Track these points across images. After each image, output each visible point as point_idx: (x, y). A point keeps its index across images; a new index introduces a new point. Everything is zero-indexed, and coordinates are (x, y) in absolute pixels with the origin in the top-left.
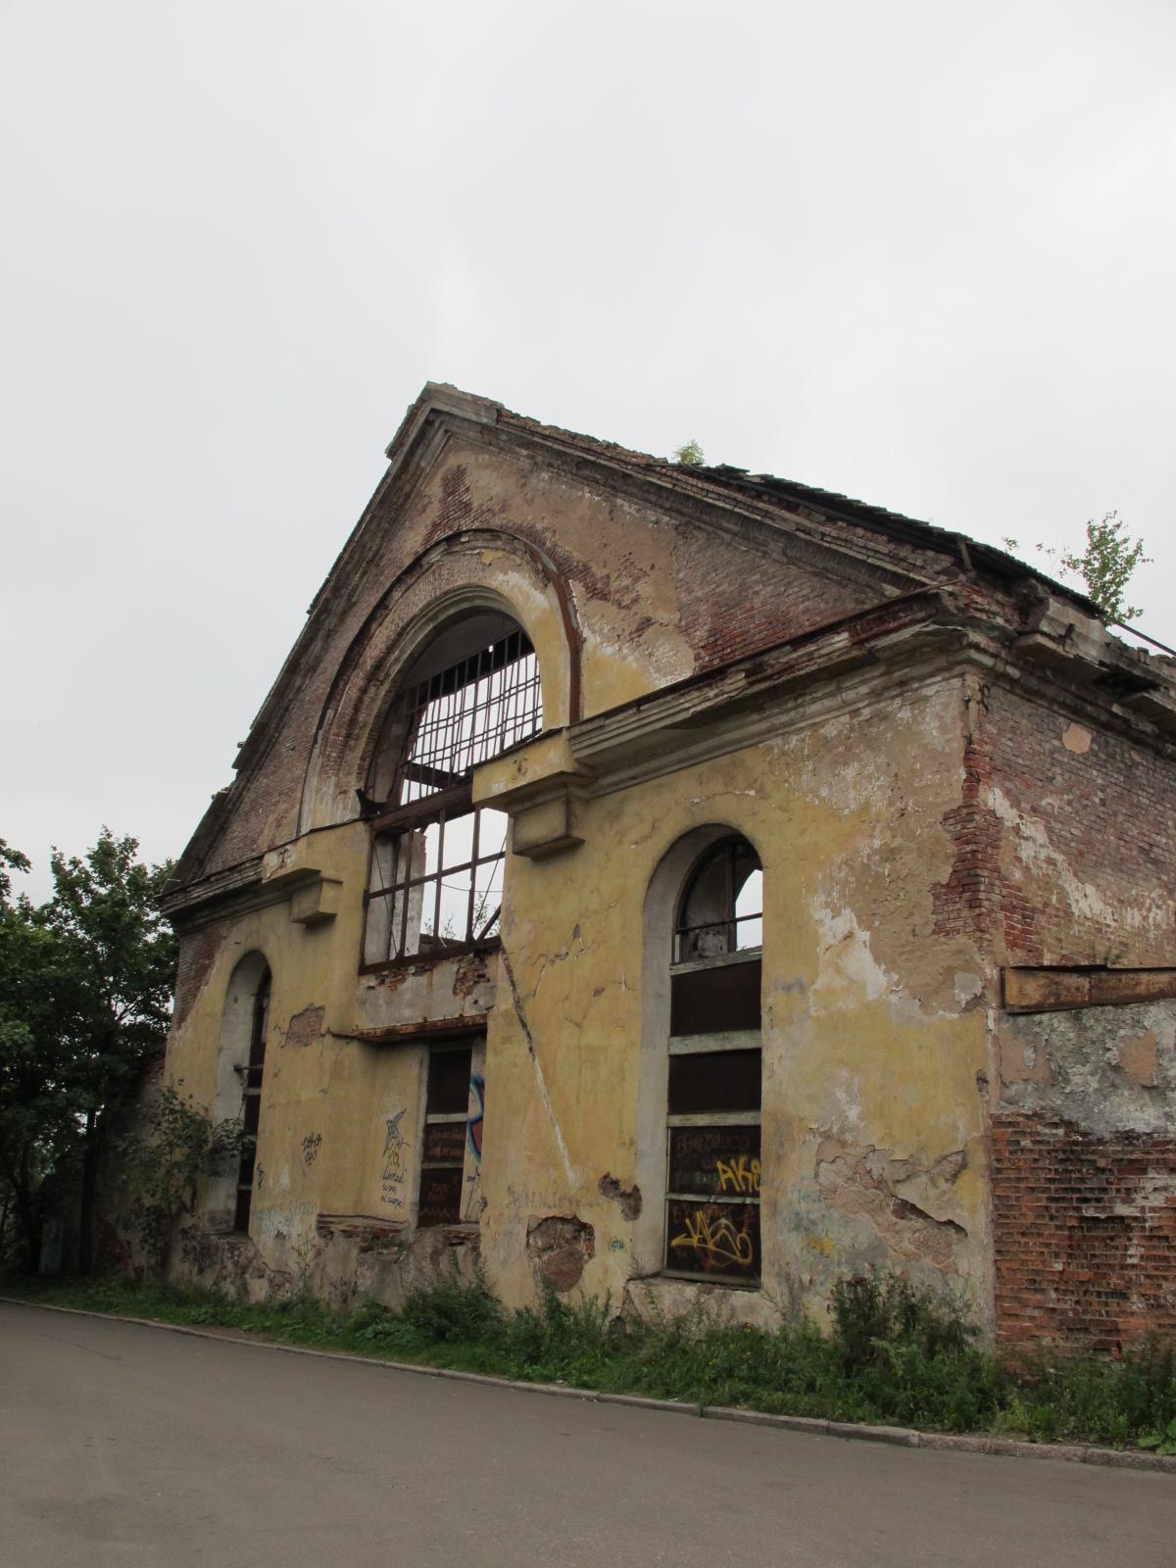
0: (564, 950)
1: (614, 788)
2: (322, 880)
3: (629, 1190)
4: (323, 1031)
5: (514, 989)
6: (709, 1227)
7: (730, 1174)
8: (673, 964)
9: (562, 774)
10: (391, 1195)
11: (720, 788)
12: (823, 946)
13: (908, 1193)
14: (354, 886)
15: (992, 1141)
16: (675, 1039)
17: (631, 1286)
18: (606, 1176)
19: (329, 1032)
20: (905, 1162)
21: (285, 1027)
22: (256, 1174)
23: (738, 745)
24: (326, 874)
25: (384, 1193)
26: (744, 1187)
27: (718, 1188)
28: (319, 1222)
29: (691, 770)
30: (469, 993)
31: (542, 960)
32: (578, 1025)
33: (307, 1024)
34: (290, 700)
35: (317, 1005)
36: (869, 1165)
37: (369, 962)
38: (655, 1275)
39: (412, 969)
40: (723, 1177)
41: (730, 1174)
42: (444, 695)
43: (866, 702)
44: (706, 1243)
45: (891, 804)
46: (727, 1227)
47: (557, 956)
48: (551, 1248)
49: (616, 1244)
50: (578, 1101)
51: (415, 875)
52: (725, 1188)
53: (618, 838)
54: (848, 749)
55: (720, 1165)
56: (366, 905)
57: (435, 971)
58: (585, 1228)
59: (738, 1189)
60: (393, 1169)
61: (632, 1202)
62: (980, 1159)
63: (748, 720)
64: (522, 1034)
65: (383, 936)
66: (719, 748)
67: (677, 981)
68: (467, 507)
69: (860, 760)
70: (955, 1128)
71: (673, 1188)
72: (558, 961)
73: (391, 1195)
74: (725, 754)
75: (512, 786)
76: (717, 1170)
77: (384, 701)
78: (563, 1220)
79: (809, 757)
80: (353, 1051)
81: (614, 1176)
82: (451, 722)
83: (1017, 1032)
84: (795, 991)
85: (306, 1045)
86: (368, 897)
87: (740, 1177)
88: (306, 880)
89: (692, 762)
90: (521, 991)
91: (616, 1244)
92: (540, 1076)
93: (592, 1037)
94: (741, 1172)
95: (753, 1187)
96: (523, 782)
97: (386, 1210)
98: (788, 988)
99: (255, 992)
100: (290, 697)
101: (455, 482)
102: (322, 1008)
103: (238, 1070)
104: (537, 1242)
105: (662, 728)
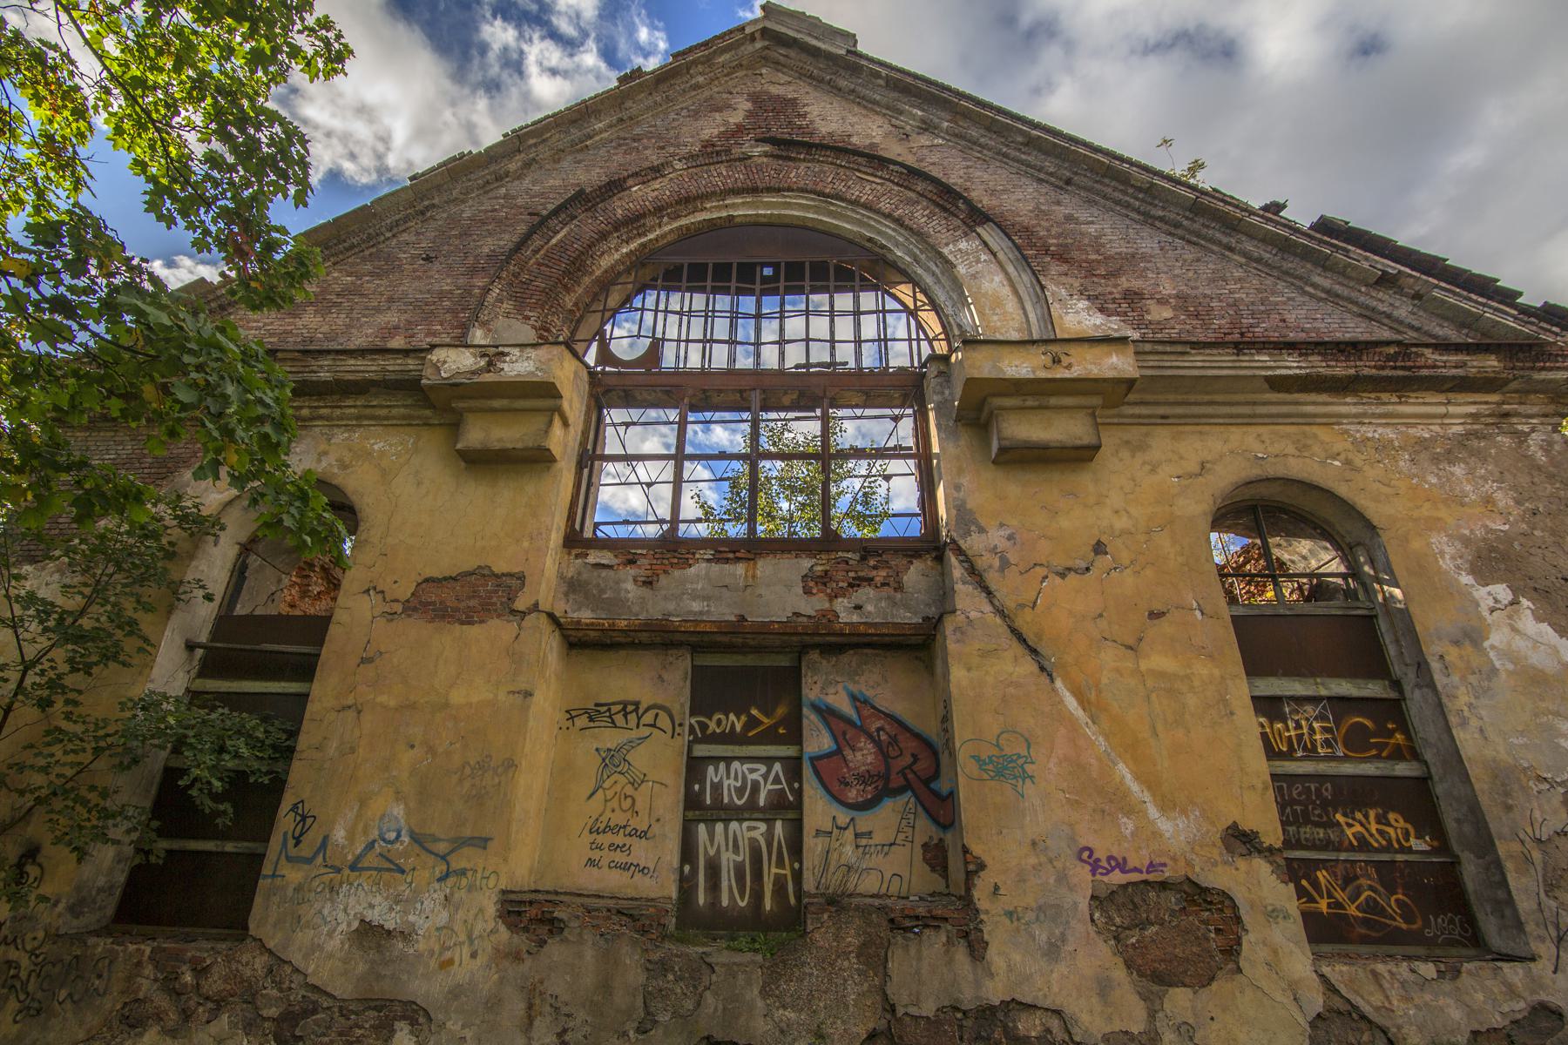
1: (1136, 421)
6: (1343, 890)
7: (1358, 828)
10: (620, 857)
18: (1235, 825)
19: (535, 608)
21: (405, 590)
23: (1310, 420)
25: (596, 855)
26: (1384, 843)
27: (1347, 843)
28: (503, 902)
31: (1041, 571)
34: (433, 206)
35: (500, 567)
40: (1349, 832)
41: (1358, 828)
43: (1462, 421)
44: (1343, 907)
46: (1371, 888)
47: (1069, 569)
48: (1143, 925)
52: (1355, 843)
53: (1148, 467)
55: (1339, 817)
57: (760, 563)
59: (1376, 845)
60: (619, 819)
63: (1348, 400)
64: (1018, 648)
72: (1072, 576)
73: (620, 857)
74: (1293, 424)
75: (1043, 374)
76: (1338, 824)
78: (1163, 885)
81: (1246, 826)
85: (462, 623)
87: (1374, 832)
92: (1071, 702)
93: (1158, 661)
94: (1373, 827)
95: (1398, 841)
96: (1060, 373)
98: (1456, 643)
99: (243, 539)
100: (436, 201)
102: (521, 577)
103: (190, 647)
104: (1110, 918)
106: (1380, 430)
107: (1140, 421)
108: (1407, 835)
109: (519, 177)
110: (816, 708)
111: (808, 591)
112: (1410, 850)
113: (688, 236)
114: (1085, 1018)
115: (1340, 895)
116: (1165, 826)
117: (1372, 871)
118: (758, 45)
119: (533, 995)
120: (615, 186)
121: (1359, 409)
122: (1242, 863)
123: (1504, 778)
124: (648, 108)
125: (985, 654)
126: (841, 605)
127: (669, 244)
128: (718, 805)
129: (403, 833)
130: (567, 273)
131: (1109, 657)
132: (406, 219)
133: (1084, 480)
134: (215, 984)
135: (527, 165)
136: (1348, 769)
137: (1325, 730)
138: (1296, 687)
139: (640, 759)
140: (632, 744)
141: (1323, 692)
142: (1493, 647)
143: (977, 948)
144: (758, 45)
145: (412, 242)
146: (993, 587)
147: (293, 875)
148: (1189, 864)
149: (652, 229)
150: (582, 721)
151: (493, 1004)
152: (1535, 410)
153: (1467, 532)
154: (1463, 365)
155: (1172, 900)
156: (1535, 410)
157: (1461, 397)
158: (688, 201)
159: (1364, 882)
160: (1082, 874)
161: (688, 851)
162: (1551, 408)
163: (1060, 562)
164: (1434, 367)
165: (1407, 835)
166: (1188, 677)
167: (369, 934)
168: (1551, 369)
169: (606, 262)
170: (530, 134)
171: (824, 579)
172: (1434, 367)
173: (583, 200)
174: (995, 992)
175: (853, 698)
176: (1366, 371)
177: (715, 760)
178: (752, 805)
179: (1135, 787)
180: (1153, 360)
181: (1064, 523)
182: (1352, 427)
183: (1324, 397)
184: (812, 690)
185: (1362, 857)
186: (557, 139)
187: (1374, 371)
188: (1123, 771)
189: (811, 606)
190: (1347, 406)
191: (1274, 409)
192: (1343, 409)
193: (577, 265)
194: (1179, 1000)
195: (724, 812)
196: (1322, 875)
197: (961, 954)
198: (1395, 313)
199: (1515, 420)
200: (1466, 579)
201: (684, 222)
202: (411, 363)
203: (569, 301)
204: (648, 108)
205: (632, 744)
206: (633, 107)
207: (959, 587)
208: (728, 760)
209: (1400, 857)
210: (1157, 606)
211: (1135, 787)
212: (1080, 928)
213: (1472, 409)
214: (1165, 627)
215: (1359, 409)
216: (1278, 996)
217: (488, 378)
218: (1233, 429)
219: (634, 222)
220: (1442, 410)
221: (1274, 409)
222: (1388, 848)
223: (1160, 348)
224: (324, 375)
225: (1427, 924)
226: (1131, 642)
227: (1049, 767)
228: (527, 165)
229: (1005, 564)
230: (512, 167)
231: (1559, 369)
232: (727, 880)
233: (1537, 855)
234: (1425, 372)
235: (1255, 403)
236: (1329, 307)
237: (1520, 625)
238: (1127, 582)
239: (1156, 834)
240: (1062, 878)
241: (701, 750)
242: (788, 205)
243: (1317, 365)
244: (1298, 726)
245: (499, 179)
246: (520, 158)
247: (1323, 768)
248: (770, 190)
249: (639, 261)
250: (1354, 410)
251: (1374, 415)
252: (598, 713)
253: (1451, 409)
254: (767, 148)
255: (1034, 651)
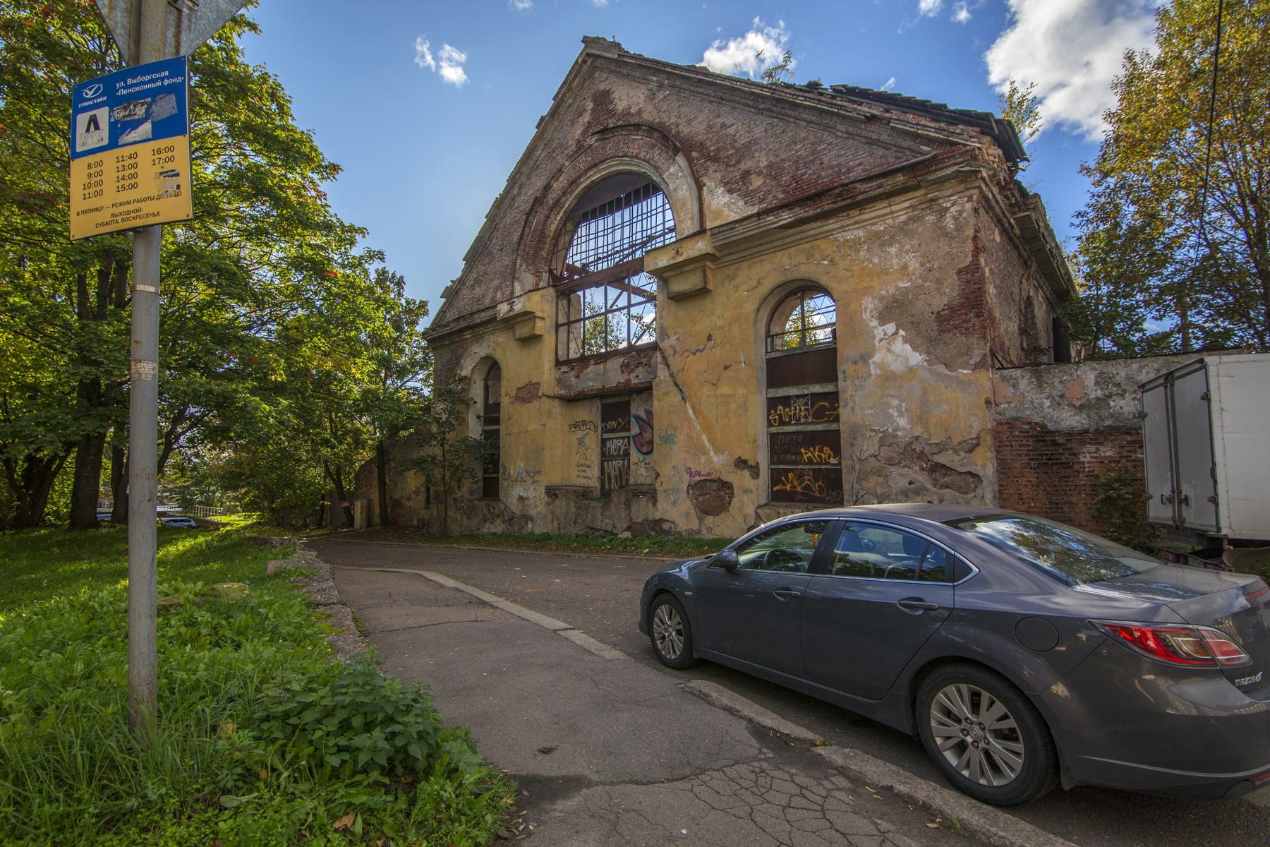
0: (702, 347)
2: (535, 317)
3: (754, 464)
4: (540, 394)
5: (548, 397)
7: (810, 454)
8: (767, 352)
9: (708, 254)
11: (804, 260)
12: (878, 339)
13: (940, 459)
14: (550, 322)
15: (996, 434)
16: (771, 390)
17: (759, 511)
19: (544, 395)
20: (937, 444)
21: (514, 394)
22: (501, 469)
23: (815, 238)
24: (538, 314)
29: (783, 252)
30: (632, 371)
31: (687, 353)
32: (714, 385)
33: (529, 393)
36: (913, 447)
37: (561, 359)
38: (767, 504)
39: (592, 362)
41: (810, 454)
42: (644, 199)
45: (922, 264)
48: (704, 495)
49: (746, 491)
50: (717, 422)
51: (572, 319)
54: (892, 237)
55: (803, 450)
56: (557, 331)
58: (726, 486)
60: (583, 462)
61: (755, 471)
62: (988, 440)
63: (831, 222)
64: (675, 390)
65: (565, 346)
66: (803, 239)
67: (769, 361)
68: (612, 113)
69: (900, 242)
70: (971, 426)
71: (772, 462)
72: (698, 353)
73: (584, 474)
75: (672, 262)
77: (559, 224)
78: (712, 481)
79: (864, 242)
80: (557, 403)
82: (654, 212)
83: (1003, 378)
84: (860, 364)
86: (558, 326)
88: (528, 316)
89: (785, 247)
90: (674, 369)
91: (746, 491)
92: (690, 411)
93: (725, 389)
96: (680, 259)
97: (582, 482)
98: (855, 363)
101: (603, 99)
102: (539, 383)
103: (479, 417)
105: (775, 228)
106: (855, 232)
107: (734, 262)
108: (830, 456)
109: (520, 194)
110: (634, 416)
111: (622, 372)
112: (829, 463)
113: (582, 198)
114: (681, 524)
115: (796, 483)
116: (715, 459)
117: (811, 473)
118: (589, 63)
119: (553, 513)
120: (547, 187)
121: (839, 224)
122: (739, 472)
123: (855, 431)
124: (554, 131)
125: (665, 394)
126: (633, 375)
127: (576, 204)
128: (610, 456)
129: (896, 414)
130: (539, 242)
131: (706, 390)
132: (492, 233)
133: (708, 303)
134: (497, 512)
135: (520, 188)
136: (810, 428)
137: (807, 410)
138: (794, 391)
139: (587, 440)
140: (585, 436)
141: (806, 392)
142: (874, 362)
143: (655, 504)
144: (589, 63)
145: (496, 242)
146: (670, 363)
147: (505, 483)
148: (721, 473)
149: (565, 203)
150: (573, 429)
151: (545, 517)
152: (950, 192)
153: (884, 292)
154: (880, 186)
155: (715, 486)
156: (950, 192)
157: (897, 199)
158: (573, 183)
159: (807, 477)
160: (687, 477)
161: (602, 471)
162: (961, 187)
163: (694, 348)
164: (865, 192)
165: (830, 456)
166: (734, 395)
167: (521, 498)
168: (942, 169)
169: (553, 228)
170: (515, 175)
171: (627, 365)
172: (865, 192)
173: (538, 201)
174: (658, 516)
175: (646, 411)
176: (826, 208)
177: (609, 439)
178: (618, 455)
179: (707, 444)
180: (721, 236)
181: (698, 327)
182: (840, 235)
183: (819, 224)
184: (633, 411)
185: (808, 467)
186: (525, 170)
187: (832, 206)
188: (704, 438)
189: (622, 378)
190: (832, 224)
191: (793, 238)
192: (830, 227)
193: (542, 235)
194: (710, 520)
195: (612, 458)
196: (790, 475)
197: (650, 505)
198: (881, 139)
199: (941, 201)
200: (874, 323)
201: (576, 192)
202: (491, 312)
203: (544, 254)
204: (554, 131)
205: (585, 436)
206: (548, 135)
207: (659, 366)
208: (612, 439)
209: (823, 467)
210: (728, 363)
211: (707, 444)
212: (684, 495)
213: (906, 204)
214: (730, 373)
215: (839, 224)
216: (739, 520)
217: (511, 314)
218: (778, 254)
219: (557, 204)
220: (888, 210)
221: (793, 238)
222: (818, 463)
223: (721, 229)
224: (478, 321)
225: (828, 495)
226: (715, 381)
227: (681, 438)
228: (520, 188)
229: (675, 352)
230: (515, 192)
231: (947, 167)
232: (613, 480)
233: (857, 466)
234: (860, 198)
235: (782, 238)
236: (851, 141)
237: (893, 348)
238: (718, 352)
239: (712, 462)
240: (680, 479)
241: (605, 436)
242: (611, 166)
243: (800, 213)
244: (795, 409)
245: (513, 199)
246: (516, 186)
247: (800, 428)
248: (601, 162)
249: (568, 217)
250: (835, 226)
251: (848, 225)
252: (576, 426)
253: (894, 208)
254: (596, 137)
255: (681, 391)
